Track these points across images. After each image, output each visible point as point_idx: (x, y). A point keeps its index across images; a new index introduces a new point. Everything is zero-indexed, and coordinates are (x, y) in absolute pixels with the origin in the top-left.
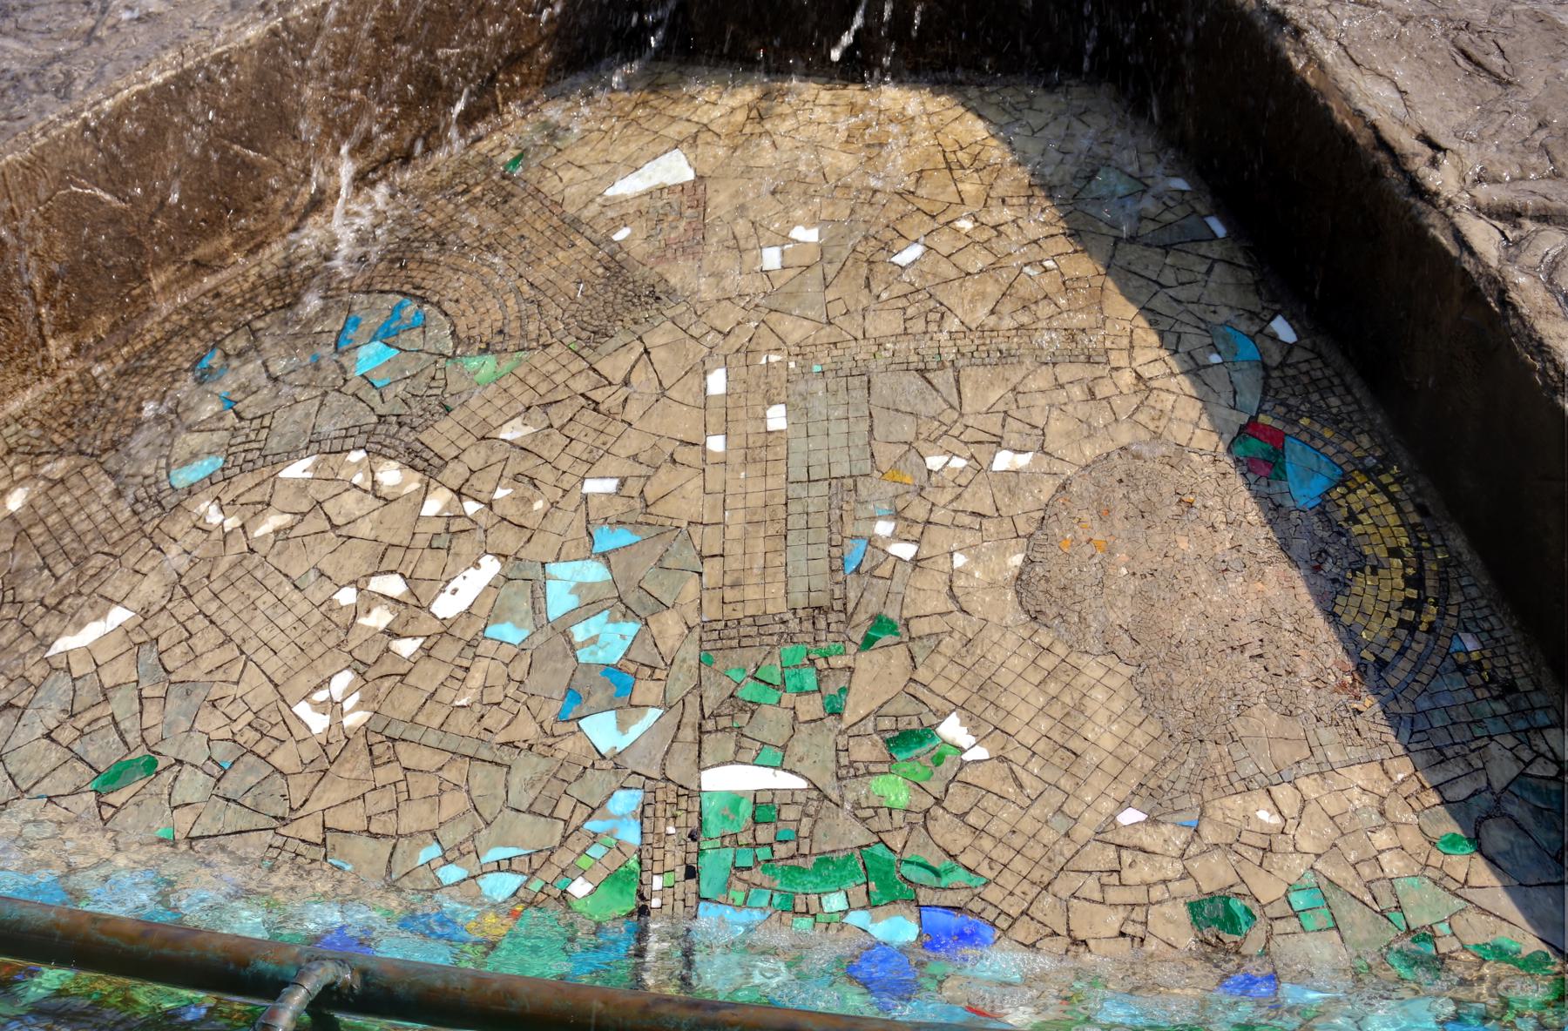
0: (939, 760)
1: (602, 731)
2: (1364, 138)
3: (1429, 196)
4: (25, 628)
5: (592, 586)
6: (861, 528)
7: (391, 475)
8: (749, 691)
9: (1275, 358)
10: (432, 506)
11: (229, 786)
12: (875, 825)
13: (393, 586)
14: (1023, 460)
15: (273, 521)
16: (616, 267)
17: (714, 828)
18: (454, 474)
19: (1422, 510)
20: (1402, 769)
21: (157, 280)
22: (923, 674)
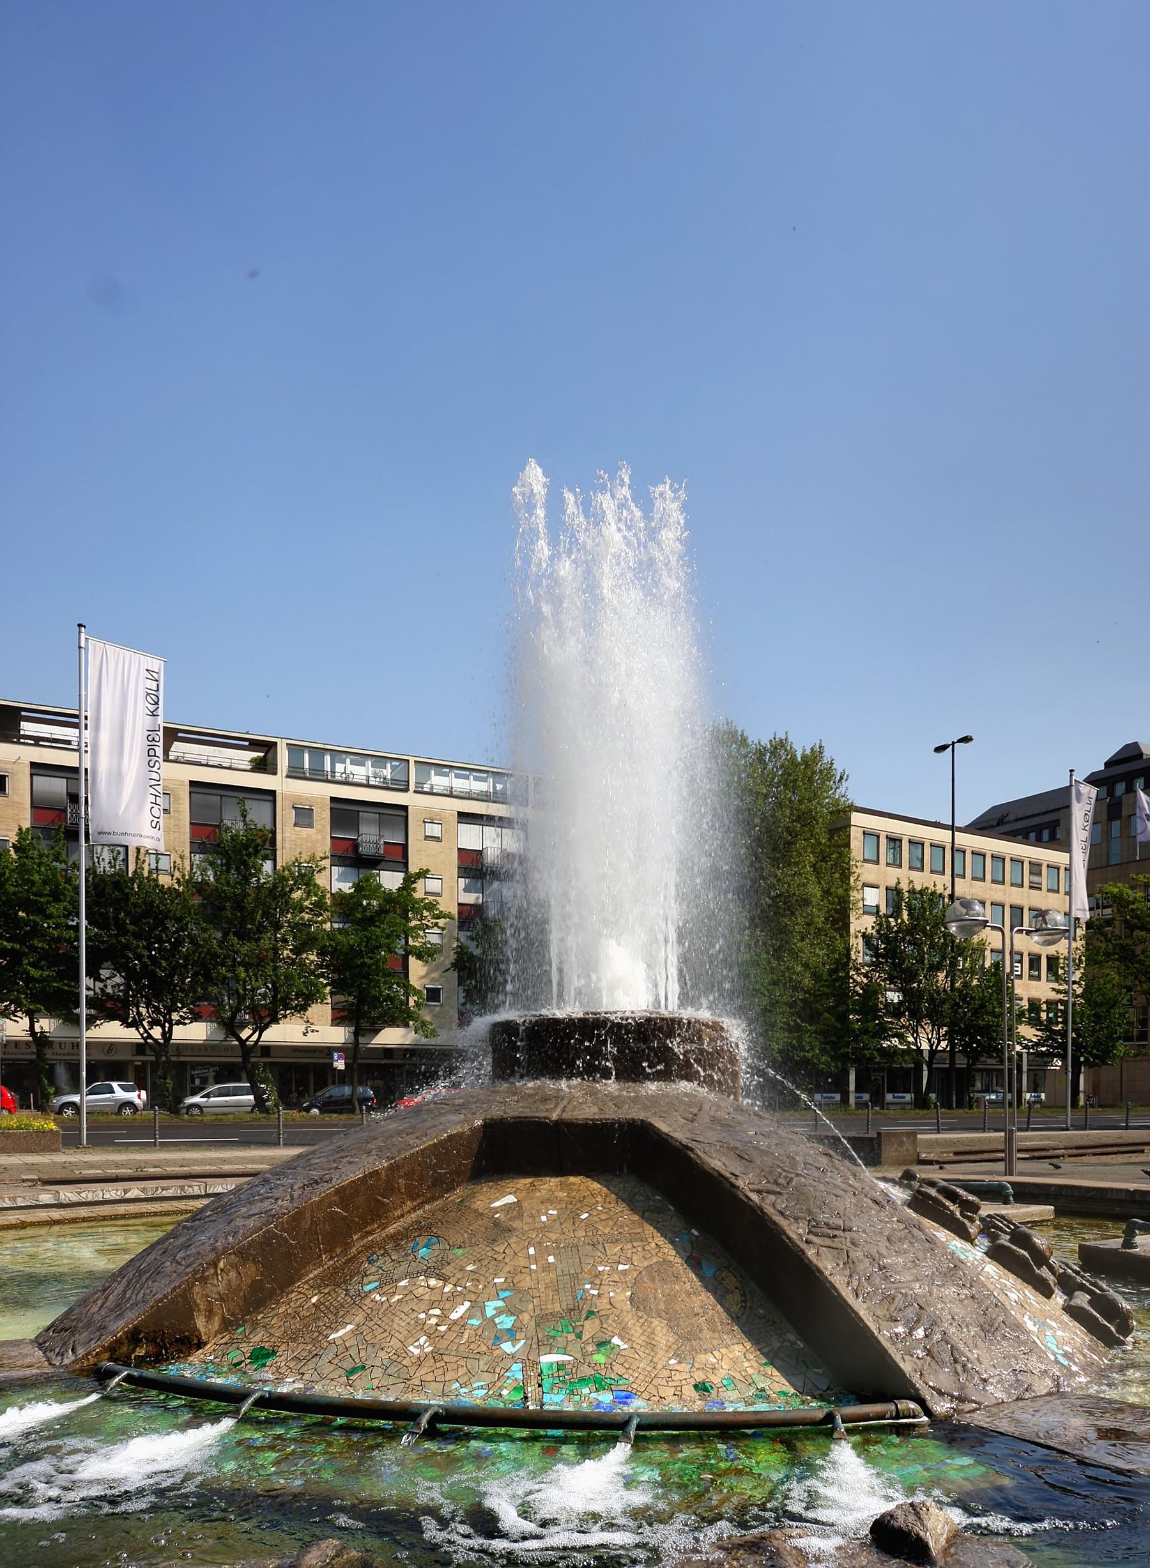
0: (613, 1349)
1: (507, 1347)
2: (716, 1174)
3: (737, 1188)
4: (320, 1333)
5: (499, 1307)
6: (581, 1287)
7: (433, 1282)
8: (552, 1333)
9: (694, 1239)
10: (447, 1289)
11: (389, 1371)
12: (596, 1368)
13: (437, 1312)
14: (626, 1267)
15: (397, 1297)
16: (496, 1224)
17: (545, 1372)
18: (453, 1280)
19: (742, 1277)
20: (748, 1345)
21: (355, 1237)
22: (605, 1326)
